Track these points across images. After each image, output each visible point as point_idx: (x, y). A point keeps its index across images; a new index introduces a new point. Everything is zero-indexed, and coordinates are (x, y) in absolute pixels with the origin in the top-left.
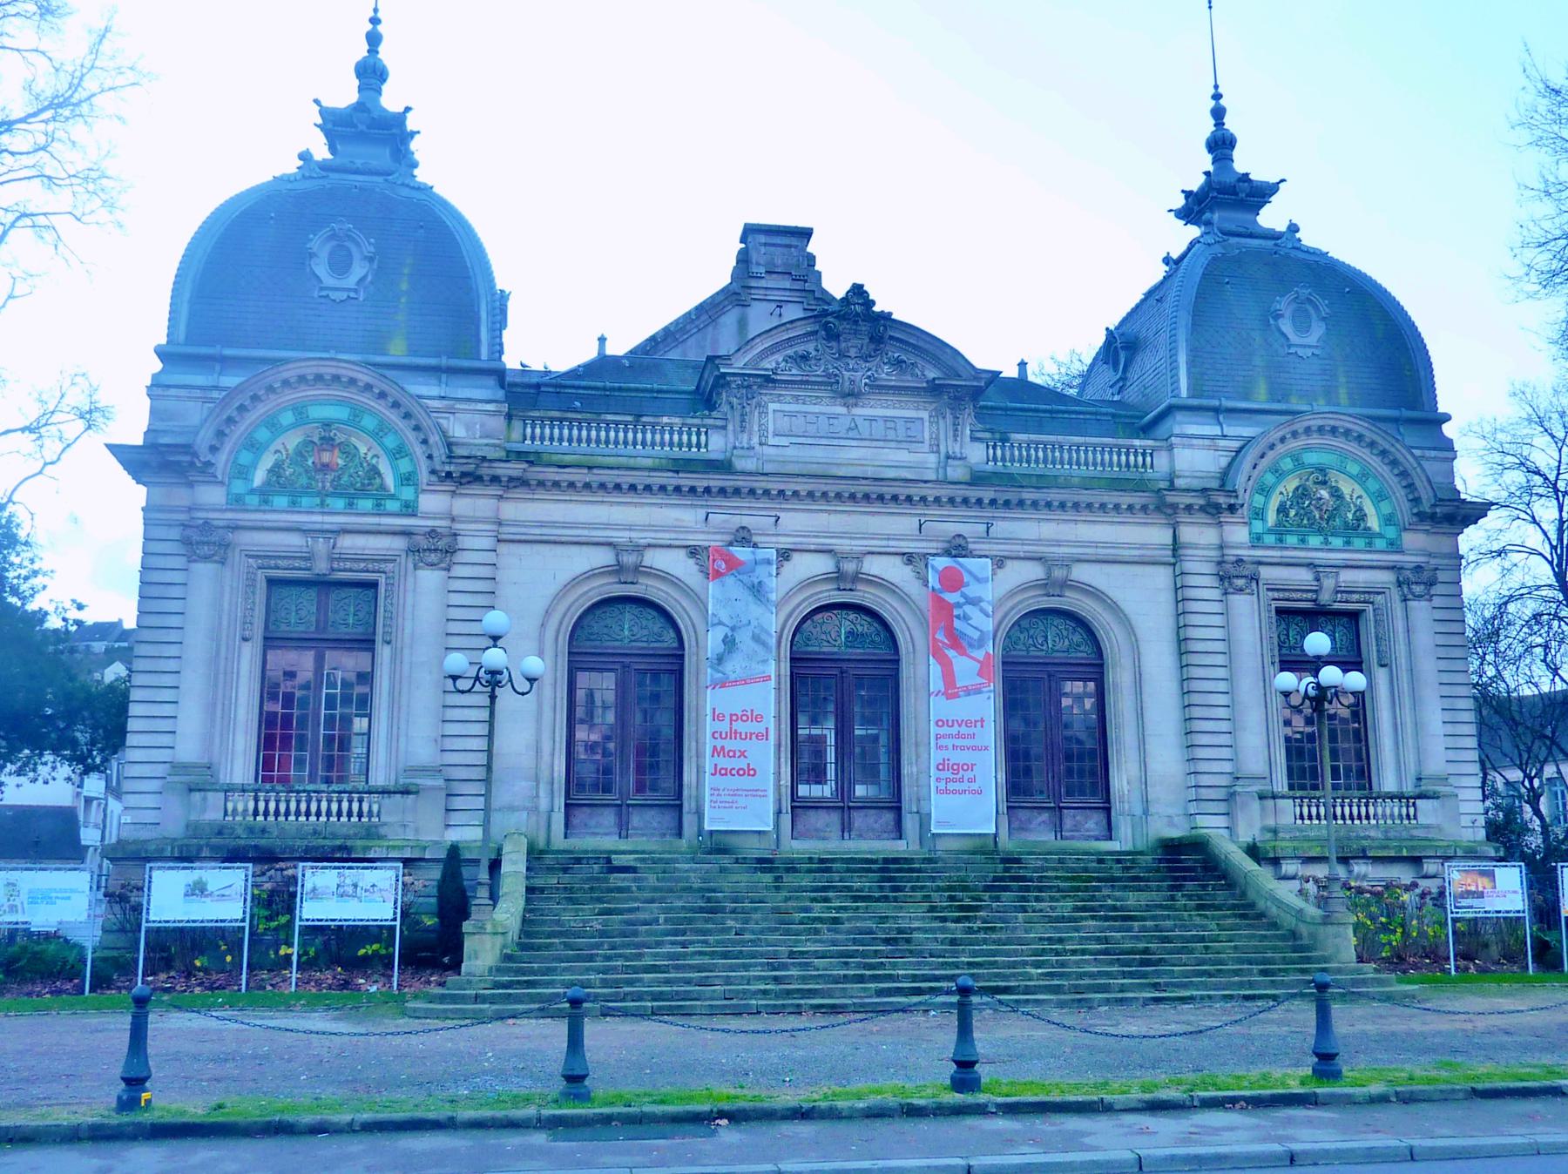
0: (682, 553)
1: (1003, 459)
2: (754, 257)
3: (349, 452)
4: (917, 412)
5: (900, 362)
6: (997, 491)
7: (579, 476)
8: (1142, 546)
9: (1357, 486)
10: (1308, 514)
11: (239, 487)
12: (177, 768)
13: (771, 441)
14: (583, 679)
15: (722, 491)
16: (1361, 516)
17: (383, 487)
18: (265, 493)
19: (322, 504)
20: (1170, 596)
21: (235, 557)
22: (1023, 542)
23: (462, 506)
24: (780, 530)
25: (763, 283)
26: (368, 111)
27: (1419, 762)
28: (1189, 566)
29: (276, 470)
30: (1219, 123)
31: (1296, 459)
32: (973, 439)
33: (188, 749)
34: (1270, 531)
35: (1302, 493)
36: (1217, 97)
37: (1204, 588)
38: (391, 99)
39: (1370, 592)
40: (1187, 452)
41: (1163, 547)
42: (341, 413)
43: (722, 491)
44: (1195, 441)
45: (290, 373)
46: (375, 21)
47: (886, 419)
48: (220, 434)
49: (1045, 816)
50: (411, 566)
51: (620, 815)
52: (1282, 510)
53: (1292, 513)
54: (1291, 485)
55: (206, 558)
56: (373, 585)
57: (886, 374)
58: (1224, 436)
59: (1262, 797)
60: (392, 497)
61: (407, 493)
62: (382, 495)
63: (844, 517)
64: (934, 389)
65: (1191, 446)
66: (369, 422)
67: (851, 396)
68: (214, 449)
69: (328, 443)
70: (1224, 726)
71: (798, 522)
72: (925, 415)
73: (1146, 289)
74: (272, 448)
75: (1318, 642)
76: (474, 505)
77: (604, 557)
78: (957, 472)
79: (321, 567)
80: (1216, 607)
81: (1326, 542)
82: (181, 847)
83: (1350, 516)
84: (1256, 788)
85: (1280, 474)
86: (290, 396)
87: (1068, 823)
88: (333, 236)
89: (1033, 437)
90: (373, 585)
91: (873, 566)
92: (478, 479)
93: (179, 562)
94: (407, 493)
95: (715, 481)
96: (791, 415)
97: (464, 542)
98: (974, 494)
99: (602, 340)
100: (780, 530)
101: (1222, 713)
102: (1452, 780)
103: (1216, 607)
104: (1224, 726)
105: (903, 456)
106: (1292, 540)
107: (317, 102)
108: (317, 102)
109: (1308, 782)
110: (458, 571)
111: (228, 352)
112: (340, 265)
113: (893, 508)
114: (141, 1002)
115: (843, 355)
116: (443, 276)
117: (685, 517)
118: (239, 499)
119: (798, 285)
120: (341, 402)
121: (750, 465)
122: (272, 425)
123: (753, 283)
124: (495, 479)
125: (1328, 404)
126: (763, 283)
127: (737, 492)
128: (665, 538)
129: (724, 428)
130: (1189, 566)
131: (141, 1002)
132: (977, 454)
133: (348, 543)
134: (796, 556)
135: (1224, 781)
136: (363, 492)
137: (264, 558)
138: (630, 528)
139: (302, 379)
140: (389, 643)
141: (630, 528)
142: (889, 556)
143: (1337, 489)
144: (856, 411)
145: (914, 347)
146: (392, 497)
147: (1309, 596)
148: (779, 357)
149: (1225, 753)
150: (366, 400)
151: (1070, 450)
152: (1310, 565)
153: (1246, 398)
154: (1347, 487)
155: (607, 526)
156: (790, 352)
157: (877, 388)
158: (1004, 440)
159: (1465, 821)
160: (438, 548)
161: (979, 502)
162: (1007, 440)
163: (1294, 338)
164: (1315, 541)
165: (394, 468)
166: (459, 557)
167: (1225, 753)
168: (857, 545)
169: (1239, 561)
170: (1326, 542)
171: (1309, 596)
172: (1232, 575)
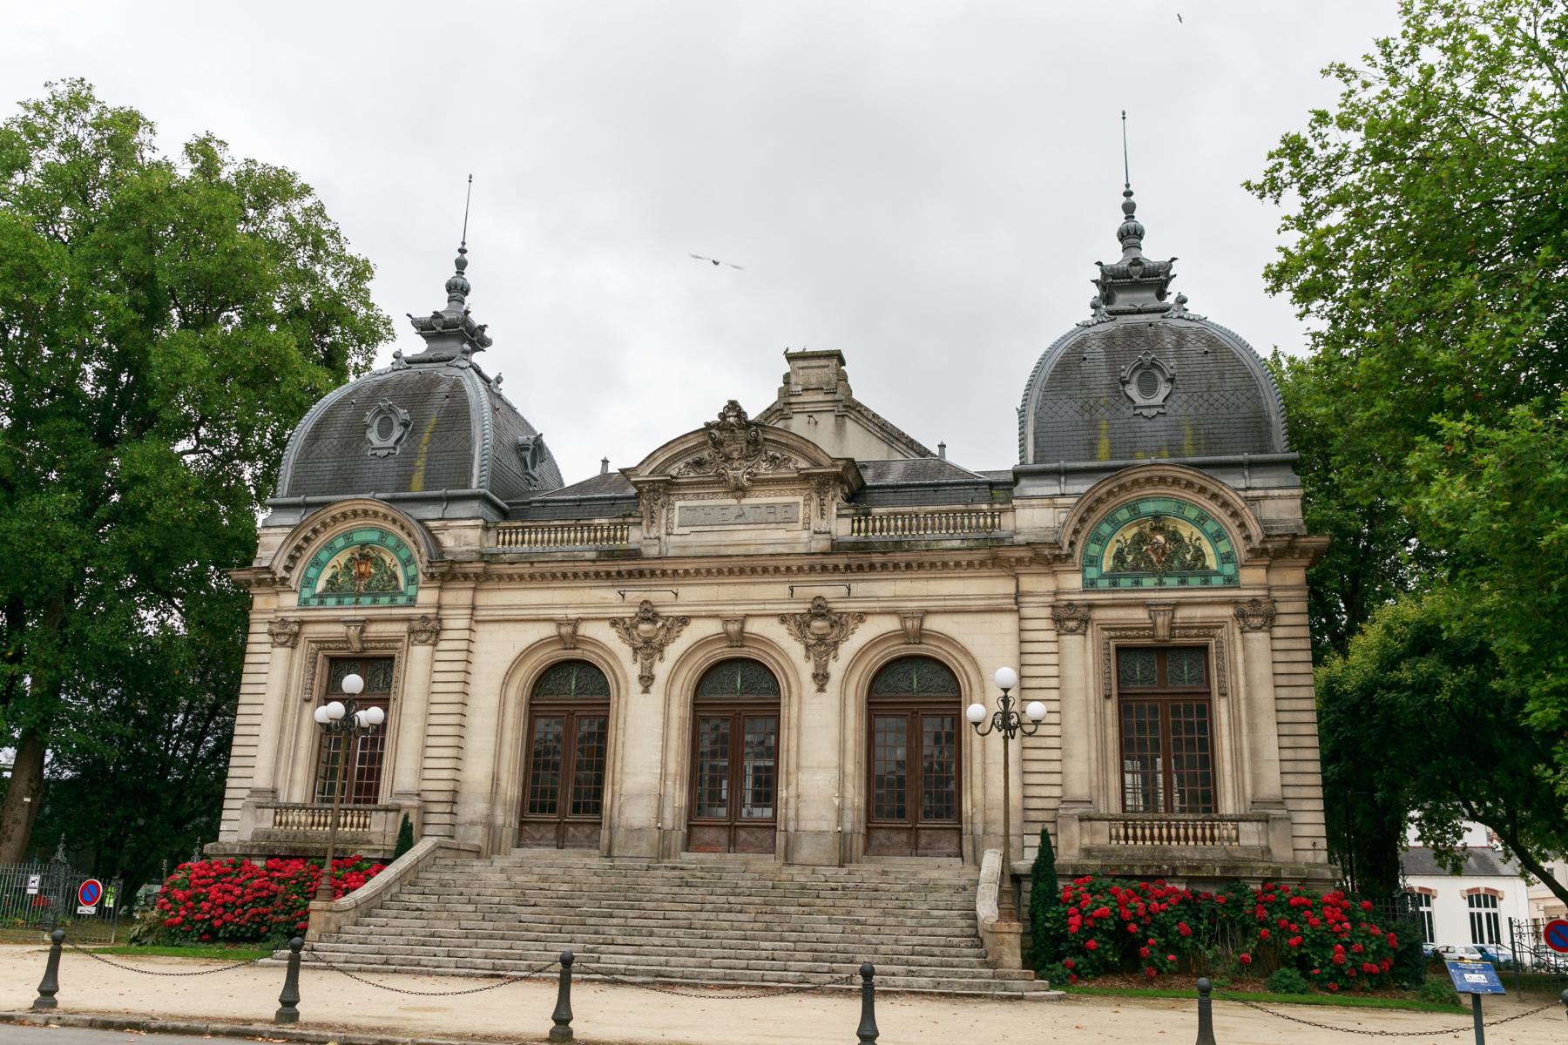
0: (607, 624)
1: (866, 530)
2: (793, 379)
3: (378, 562)
4: (793, 497)
5: (774, 458)
6: (855, 558)
7: (525, 569)
8: (989, 597)
9: (1195, 530)
10: (1145, 558)
11: (307, 593)
12: (255, 792)
13: (676, 531)
14: (880, 723)
15: (630, 574)
16: (1199, 555)
17: (397, 587)
18: (321, 598)
19: (357, 602)
20: (1014, 640)
21: (302, 643)
22: (878, 599)
23: (1276, 579)
24: (679, 601)
25: (801, 399)
26: (1141, 264)
27: (1255, 787)
28: (1026, 612)
29: (332, 582)
30: (460, 272)
31: (347, 536)
32: (839, 516)
33: (262, 780)
34: (1103, 576)
35: (1140, 539)
36: (1128, 194)
38: (1152, 252)
39: (1208, 628)
40: (1028, 512)
41: (1006, 596)
42: (373, 536)
43: (630, 574)
44: (1034, 502)
45: (336, 511)
46: (1128, 194)
47: (769, 506)
48: (292, 558)
49: (903, 837)
50: (1237, 631)
51: (557, 830)
52: (1119, 557)
53: (1130, 558)
54: (1130, 533)
55: (1072, 631)
56: (1204, 649)
57: (764, 470)
58: (1063, 495)
59: (1081, 820)
60: (402, 594)
61: (1229, 569)
62: (1206, 575)
63: (732, 588)
64: (805, 478)
65: (1031, 506)
66: (391, 542)
67: (740, 491)
68: (288, 569)
69: (365, 558)
70: (1055, 754)
71: (692, 595)
72: (800, 499)
73: (515, 405)
74: (1114, 539)
75: (353, 683)
76: (459, 596)
77: (548, 630)
78: (822, 544)
79: (1162, 632)
80: (1052, 647)
81: (1161, 583)
82: (1523, 875)
83: (1188, 557)
84: (1079, 810)
85: (1117, 525)
86: (342, 527)
87: (923, 841)
88: (381, 411)
89: (930, 508)
90: (392, 658)
91: (754, 627)
92: (454, 578)
93: (267, 648)
94: (1229, 569)
95: (625, 566)
96: (694, 509)
97: (448, 624)
98: (830, 561)
99: (605, 462)
100: (679, 601)
101: (1054, 742)
102: (1291, 805)
103: (1052, 647)
104: (1055, 754)
105: (781, 535)
106: (1125, 583)
107: (1099, 264)
108: (1099, 264)
109: (1201, 806)
110: (442, 645)
111: (309, 499)
112: (385, 432)
113: (971, 572)
114: (57, 941)
115: (728, 458)
116: (740, 414)
117: (604, 597)
118: (1093, 583)
119: (829, 397)
120: (373, 529)
121: (654, 551)
122: (1110, 519)
123: (793, 400)
124: (466, 577)
125: (1172, 456)
126: (801, 399)
127: (641, 574)
128: (593, 612)
129: (640, 524)
130: (1026, 612)
131: (1205, 992)
132: (843, 529)
133: (1183, 614)
134: (693, 622)
135: (1052, 804)
136: (383, 592)
137: (322, 643)
138: (566, 606)
139: (344, 516)
140: (1224, 695)
141: (566, 606)
142: (767, 616)
143: (1175, 533)
144: (744, 501)
145: (786, 445)
146: (402, 594)
147: (1146, 633)
148: (681, 464)
149: (1056, 779)
150: (388, 526)
151: (925, 518)
152: (1145, 605)
153: (1092, 457)
154: (1186, 531)
155: (552, 606)
156: (689, 460)
157: (757, 482)
158: (867, 514)
159: (1307, 844)
160: (430, 629)
161: (836, 568)
162: (869, 514)
163: (1139, 401)
164: (1149, 582)
165: (1216, 549)
166: (445, 635)
167: (1056, 779)
168: (740, 610)
169: (1070, 605)
170: (1161, 583)
171: (1146, 633)
172: (1068, 618)
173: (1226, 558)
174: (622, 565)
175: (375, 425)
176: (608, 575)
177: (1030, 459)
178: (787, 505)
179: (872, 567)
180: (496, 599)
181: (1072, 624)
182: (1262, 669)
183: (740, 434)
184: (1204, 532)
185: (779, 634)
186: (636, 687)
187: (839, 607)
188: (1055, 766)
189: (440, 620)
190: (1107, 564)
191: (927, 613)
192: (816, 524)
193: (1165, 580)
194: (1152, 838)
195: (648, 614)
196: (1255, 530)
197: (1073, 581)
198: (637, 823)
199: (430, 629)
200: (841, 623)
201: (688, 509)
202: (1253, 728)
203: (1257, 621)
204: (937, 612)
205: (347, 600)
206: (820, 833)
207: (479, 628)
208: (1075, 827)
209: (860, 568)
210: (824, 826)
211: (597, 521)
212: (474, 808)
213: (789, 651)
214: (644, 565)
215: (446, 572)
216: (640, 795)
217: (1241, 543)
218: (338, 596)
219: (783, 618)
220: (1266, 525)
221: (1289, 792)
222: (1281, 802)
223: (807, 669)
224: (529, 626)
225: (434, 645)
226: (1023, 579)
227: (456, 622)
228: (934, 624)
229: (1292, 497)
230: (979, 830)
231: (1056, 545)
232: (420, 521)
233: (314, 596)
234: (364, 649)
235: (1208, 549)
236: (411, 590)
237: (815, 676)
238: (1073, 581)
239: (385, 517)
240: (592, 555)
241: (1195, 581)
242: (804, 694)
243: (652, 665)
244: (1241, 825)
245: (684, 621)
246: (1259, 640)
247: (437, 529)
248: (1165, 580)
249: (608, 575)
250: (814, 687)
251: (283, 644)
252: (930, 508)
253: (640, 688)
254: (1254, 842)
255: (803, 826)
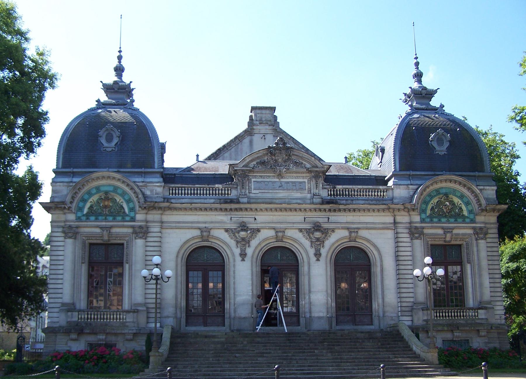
9: (459, 200)
11: (79, 214)
12: (63, 304)
13: (253, 191)
14: (191, 273)
15: (236, 210)
17: (124, 212)
21: (79, 237)
35: (439, 203)
37: (405, 237)
39: (125, 235)
50: (474, 239)
61: (472, 216)
68: (71, 203)
69: (107, 199)
71: (263, 218)
80: (409, 244)
83: (457, 211)
95: (234, 206)
103: (409, 244)
110: (149, 239)
111: (75, 170)
118: (424, 219)
121: (245, 200)
124: (160, 208)
129: (237, 188)
141: (205, 223)
143: (452, 201)
146: (127, 215)
148: (255, 163)
155: (198, 222)
156: (258, 161)
160: (142, 232)
164: (443, 220)
167: (411, 295)
173: (470, 212)
174: (229, 204)
175: (104, 136)
176: (226, 209)
177: (398, 169)
178: (300, 183)
179: (340, 210)
180: (171, 217)
181: (417, 235)
182: (483, 254)
183: (283, 152)
184: (463, 201)
185: (299, 236)
186: (238, 258)
187: (325, 226)
188: (411, 290)
189: (148, 228)
190: (428, 212)
191: (359, 229)
192: (314, 191)
193: (450, 219)
194: (449, 316)
195: (243, 227)
196: (483, 202)
197: (417, 218)
198: (243, 315)
199: (142, 232)
200: (326, 232)
201: (257, 182)
202: (480, 276)
203: (481, 236)
204: (363, 229)
205: (100, 218)
206: (319, 318)
207: (164, 231)
208: (421, 313)
209: (335, 211)
210: (321, 315)
211: (217, 186)
212: (169, 311)
213: (303, 246)
214: (242, 206)
215: (149, 205)
216: (243, 304)
217: (477, 206)
218: (95, 216)
219: (301, 230)
220: (487, 199)
221: (493, 299)
222: (489, 302)
223: (312, 252)
224: (187, 231)
225: (146, 239)
226: (412, 217)
227: (155, 229)
228: (363, 233)
229: (493, 190)
230: (381, 314)
231: (63, 203)
232: (134, 182)
233: (84, 215)
234: (109, 240)
235: (464, 208)
236: (132, 214)
237: (241, 255)
238: (71, 217)
239: (119, 180)
240: (173, 201)
241: (460, 220)
242: (311, 262)
243: (245, 249)
244: (479, 311)
245: (258, 230)
246: (482, 242)
247: (142, 186)
248: (450, 219)
249: (226, 209)
250: (315, 259)
251: (70, 238)
252: (179, 185)
253: (241, 259)
254: (483, 317)
255: (313, 315)
